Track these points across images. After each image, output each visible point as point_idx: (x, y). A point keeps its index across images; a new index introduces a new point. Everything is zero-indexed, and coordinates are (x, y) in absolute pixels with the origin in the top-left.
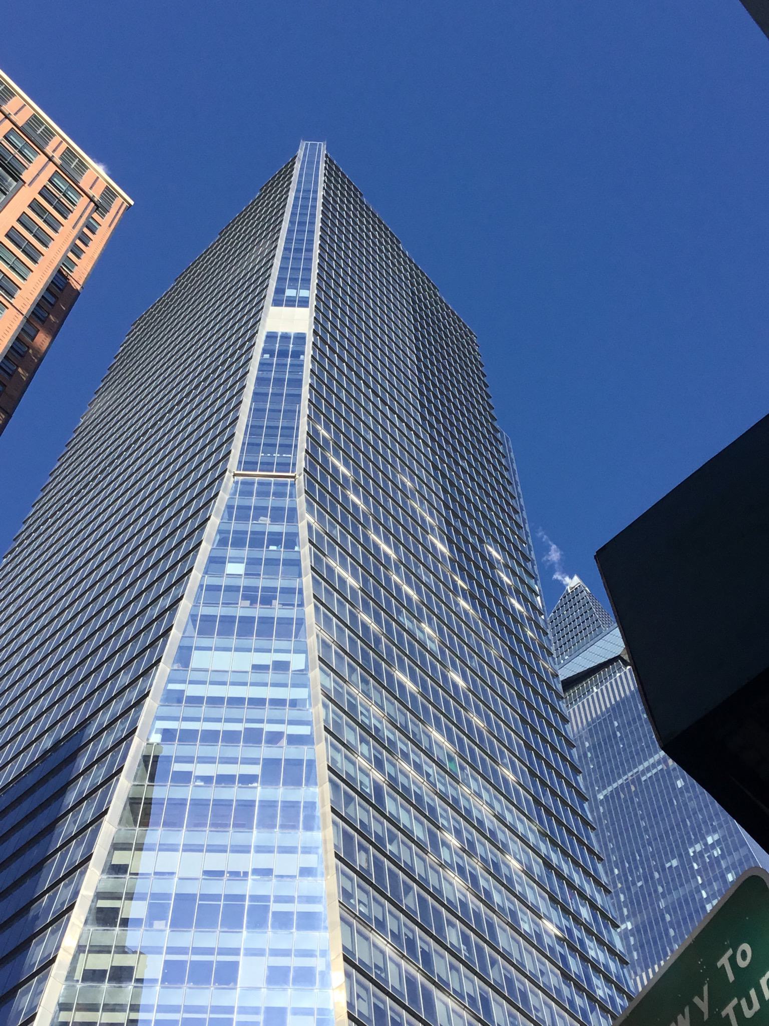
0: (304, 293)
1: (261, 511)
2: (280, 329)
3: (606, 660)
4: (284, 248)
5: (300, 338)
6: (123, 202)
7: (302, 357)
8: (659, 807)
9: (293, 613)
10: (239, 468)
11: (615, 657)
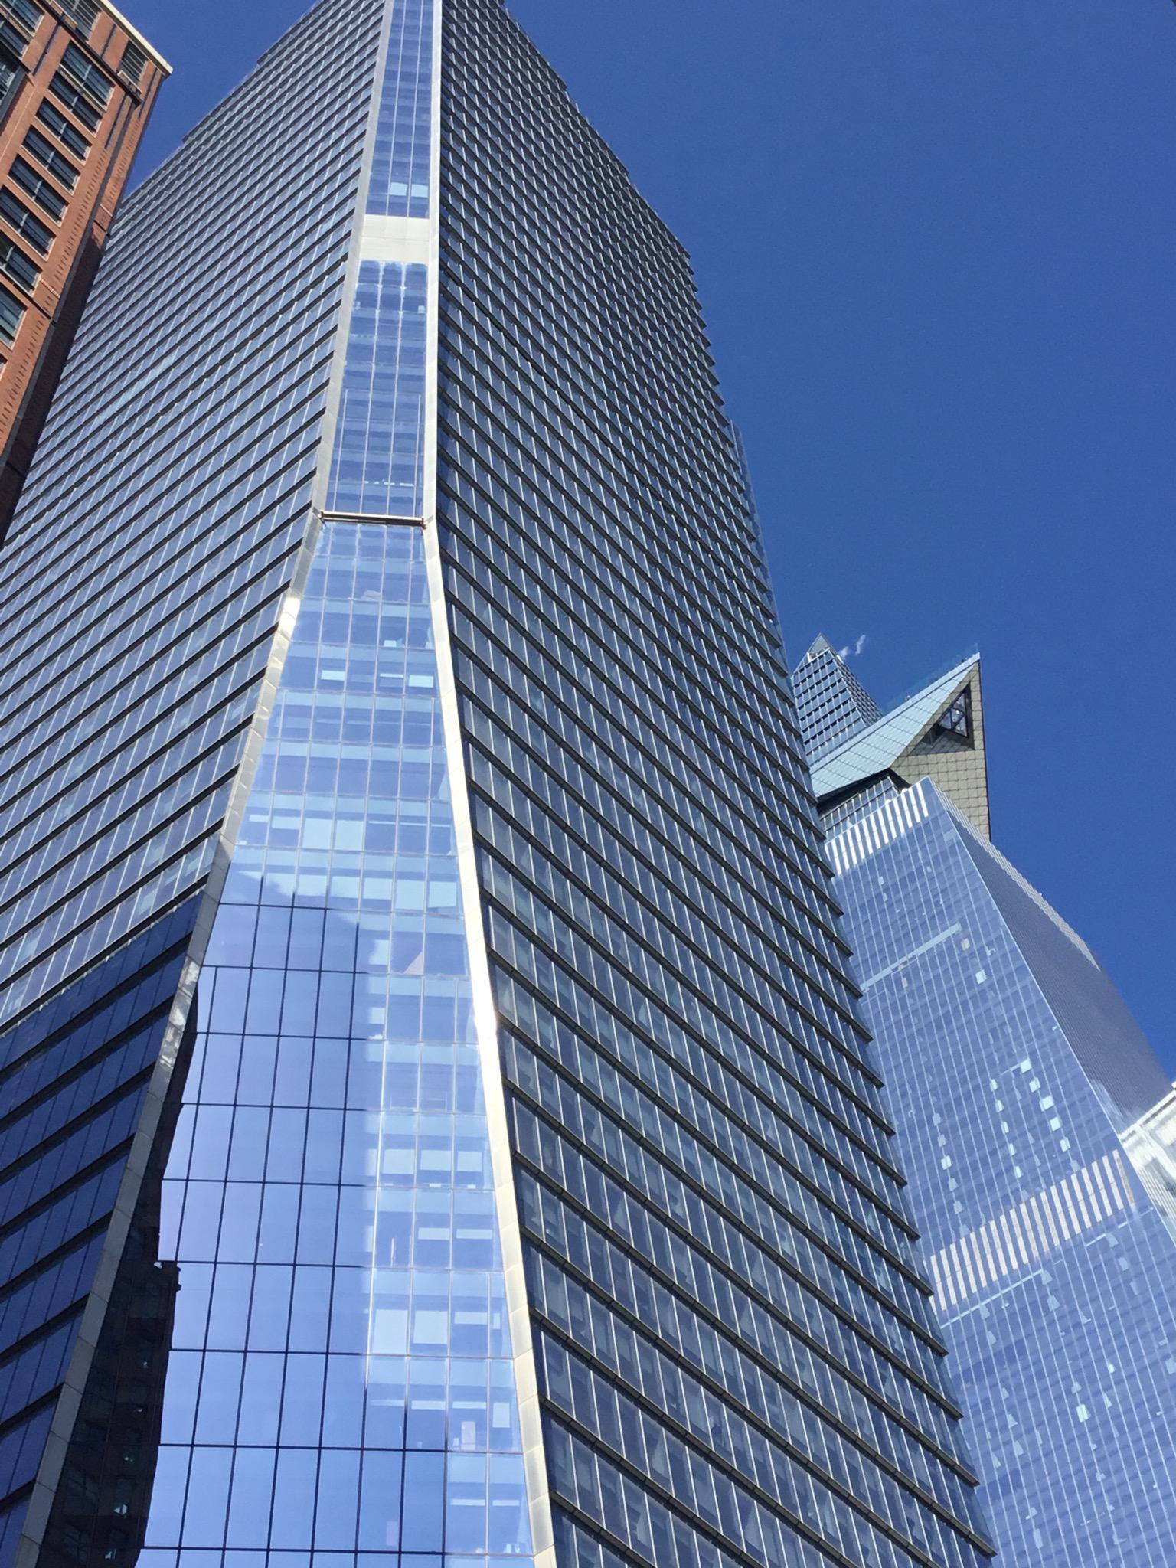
0: (418, 191)
1: (368, 580)
2: (384, 257)
3: (868, 775)
4: (381, 105)
5: (418, 274)
6: (156, 70)
7: (421, 308)
8: (965, 1047)
9: (425, 755)
10: (328, 506)
11: (882, 772)
